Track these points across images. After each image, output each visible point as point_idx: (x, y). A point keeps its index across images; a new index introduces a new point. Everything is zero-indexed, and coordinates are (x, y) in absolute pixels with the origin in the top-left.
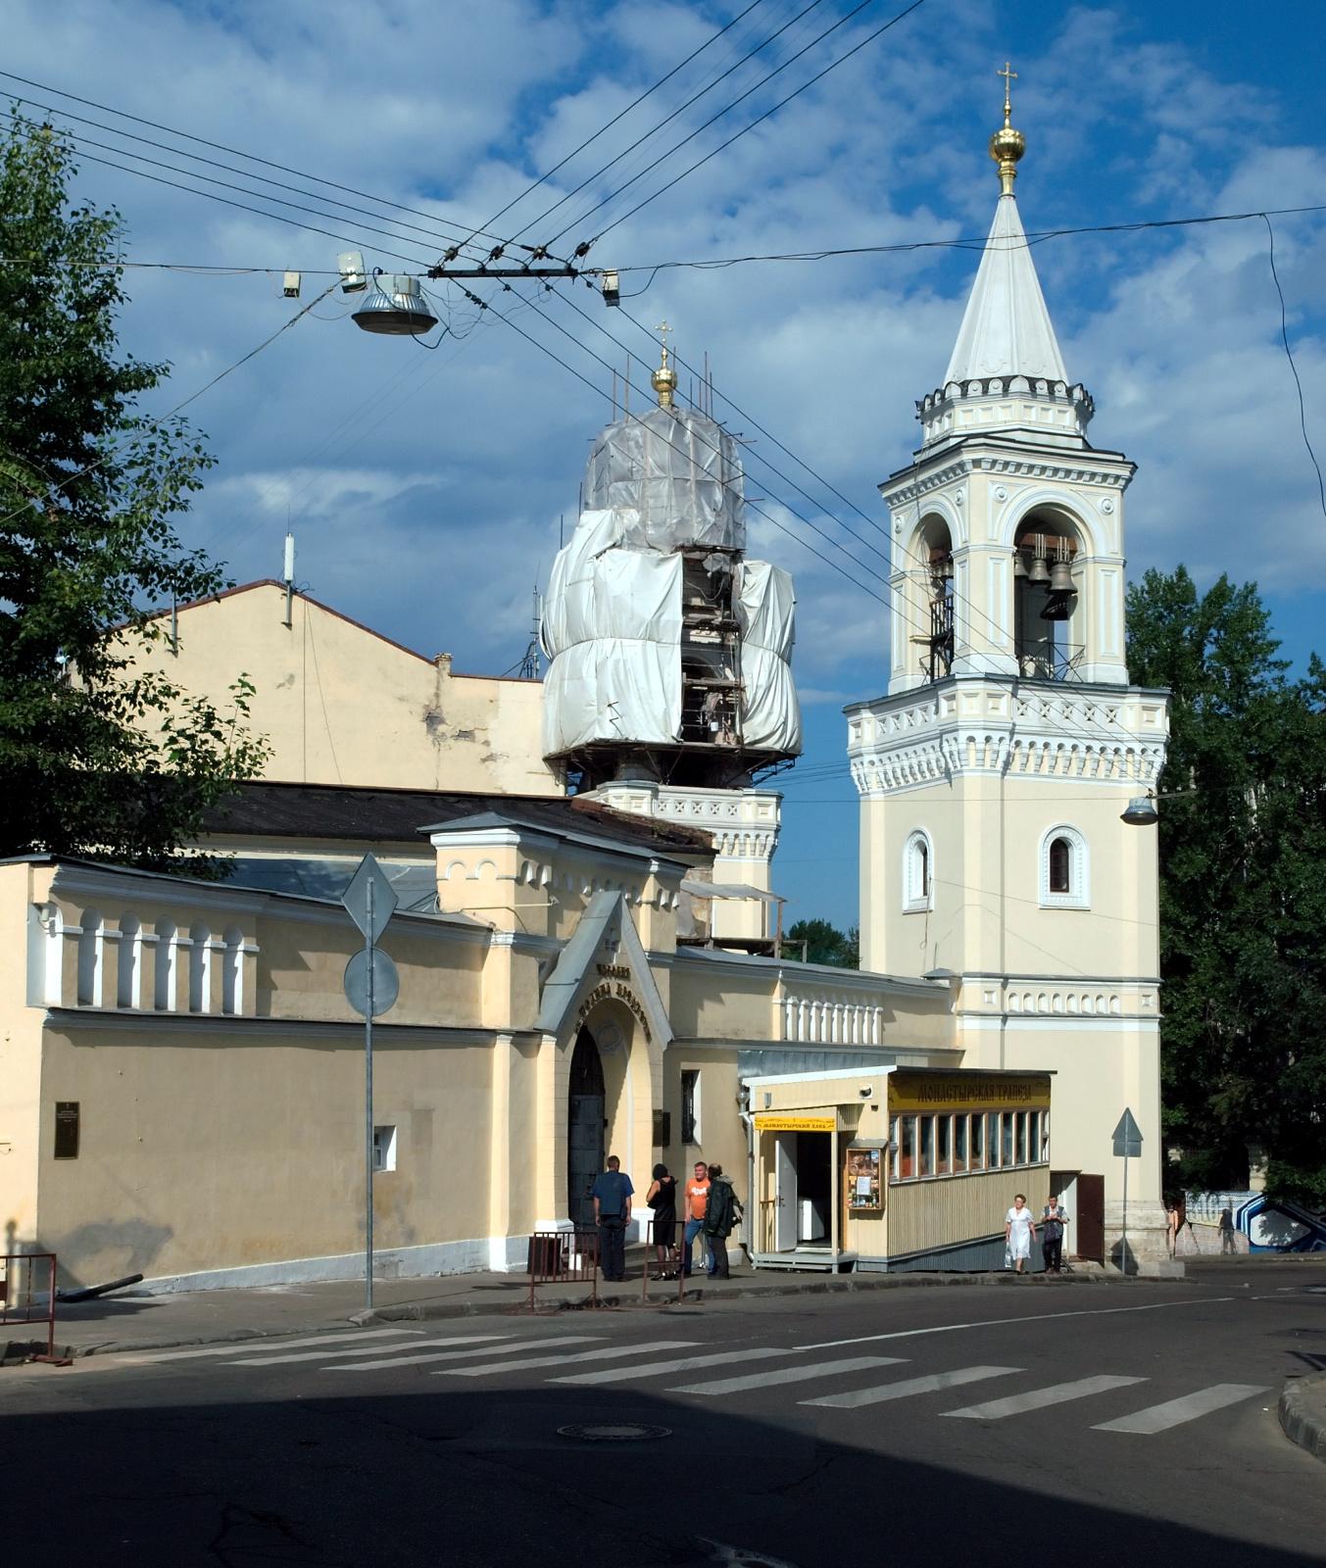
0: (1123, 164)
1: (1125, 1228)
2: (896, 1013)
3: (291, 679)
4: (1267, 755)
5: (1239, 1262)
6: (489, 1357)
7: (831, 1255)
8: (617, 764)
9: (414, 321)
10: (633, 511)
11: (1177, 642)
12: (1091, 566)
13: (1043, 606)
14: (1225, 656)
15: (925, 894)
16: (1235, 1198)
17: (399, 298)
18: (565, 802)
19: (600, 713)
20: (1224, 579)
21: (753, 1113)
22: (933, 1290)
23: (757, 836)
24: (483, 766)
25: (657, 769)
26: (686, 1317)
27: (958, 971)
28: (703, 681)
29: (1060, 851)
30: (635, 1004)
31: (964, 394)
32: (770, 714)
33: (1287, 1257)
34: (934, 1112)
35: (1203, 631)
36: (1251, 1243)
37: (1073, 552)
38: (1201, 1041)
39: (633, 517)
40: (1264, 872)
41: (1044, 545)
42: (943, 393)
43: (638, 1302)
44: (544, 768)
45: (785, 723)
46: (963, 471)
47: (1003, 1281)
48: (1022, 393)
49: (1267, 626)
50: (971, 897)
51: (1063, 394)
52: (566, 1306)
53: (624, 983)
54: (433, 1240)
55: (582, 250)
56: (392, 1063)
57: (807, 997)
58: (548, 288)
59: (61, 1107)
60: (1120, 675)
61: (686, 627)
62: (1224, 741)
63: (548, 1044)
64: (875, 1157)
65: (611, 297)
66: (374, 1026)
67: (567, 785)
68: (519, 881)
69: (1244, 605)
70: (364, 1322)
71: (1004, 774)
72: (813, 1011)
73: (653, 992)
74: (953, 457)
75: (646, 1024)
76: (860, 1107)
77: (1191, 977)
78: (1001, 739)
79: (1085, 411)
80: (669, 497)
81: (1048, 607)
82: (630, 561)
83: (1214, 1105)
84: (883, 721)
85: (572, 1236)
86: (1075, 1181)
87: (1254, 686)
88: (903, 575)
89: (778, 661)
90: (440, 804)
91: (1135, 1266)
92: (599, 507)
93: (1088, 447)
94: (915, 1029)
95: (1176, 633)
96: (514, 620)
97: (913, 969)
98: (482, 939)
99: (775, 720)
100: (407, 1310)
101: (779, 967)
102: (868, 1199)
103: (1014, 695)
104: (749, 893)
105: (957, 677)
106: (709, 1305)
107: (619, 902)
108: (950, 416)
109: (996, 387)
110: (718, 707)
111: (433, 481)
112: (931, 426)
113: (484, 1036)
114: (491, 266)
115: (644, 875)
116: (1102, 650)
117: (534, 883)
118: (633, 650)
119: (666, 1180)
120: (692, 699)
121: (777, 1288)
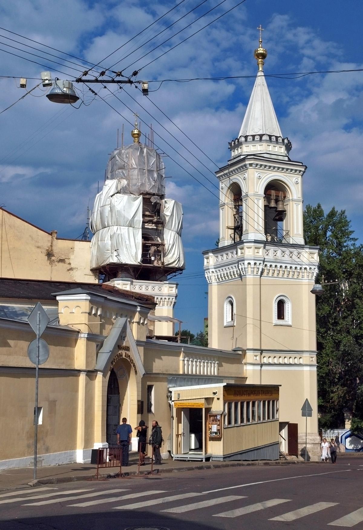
0: (291, 67)
1: (306, 444)
2: (223, 363)
4: (350, 271)
5: (342, 455)
6: (87, 499)
7: (202, 455)
8: (118, 272)
9: (70, 98)
10: (124, 180)
11: (318, 231)
12: (291, 202)
13: (274, 216)
15: (232, 320)
16: (340, 432)
17: (65, 89)
18: (100, 285)
19: (112, 253)
20: (334, 209)
21: (173, 401)
22: (241, 468)
23: (169, 299)
24: (68, 272)
25: (132, 274)
26: (156, 480)
27: (245, 348)
28: (150, 242)
29: (281, 304)
30: (132, 360)
31: (246, 140)
32: (174, 254)
33: (359, 453)
34: (239, 401)
36: (346, 449)
37: (285, 197)
38: (327, 374)
39: (124, 182)
40: (349, 313)
41: (275, 195)
42: (238, 140)
43: (136, 474)
44: (91, 273)
45: (179, 257)
46: (246, 167)
47: (266, 464)
48: (266, 140)
49: (350, 226)
50: (249, 321)
51: (281, 141)
52: (110, 477)
53: (127, 352)
54: (55, 451)
55: (135, 73)
56: (45, 382)
57: (196, 358)
58: (121, 88)
60: (301, 241)
61: (144, 222)
62: (335, 267)
63: (100, 375)
64: (219, 417)
65: (145, 91)
66: (39, 369)
67: (99, 279)
68: (90, 314)
70: (34, 485)
71: (261, 276)
72: (194, 363)
73: (137, 356)
74: (243, 162)
75: (135, 367)
76: (213, 398)
77: (324, 351)
78: (260, 264)
79: (288, 147)
80: (138, 176)
81: (276, 216)
82: (124, 198)
83: (332, 397)
84: (217, 257)
85: (108, 449)
86: (287, 426)
87: (345, 247)
88: (224, 204)
89: (177, 235)
90: (53, 285)
91: (309, 458)
92: (112, 178)
93: (289, 160)
94: (229, 369)
95: (317, 228)
96: (78, 221)
97: (228, 347)
98: (75, 336)
99: (176, 256)
100: (50, 480)
101: (182, 346)
102: (216, 433)
103: (264, 248)
104: (167, 319)
105: (244, 241)
106: (163, 475)
107: (126, 322)
108: (241, 148)
109: (257, 138)
110: (155, 251)
111: (48, 171)
112: (234, 151)
113: (76, 372)
115: (134, 313)
116: (295, 232)
117: (95, 315)
118: (124, 230)
119: (144, 427)
120: (145, 248)
121: (186, 468)
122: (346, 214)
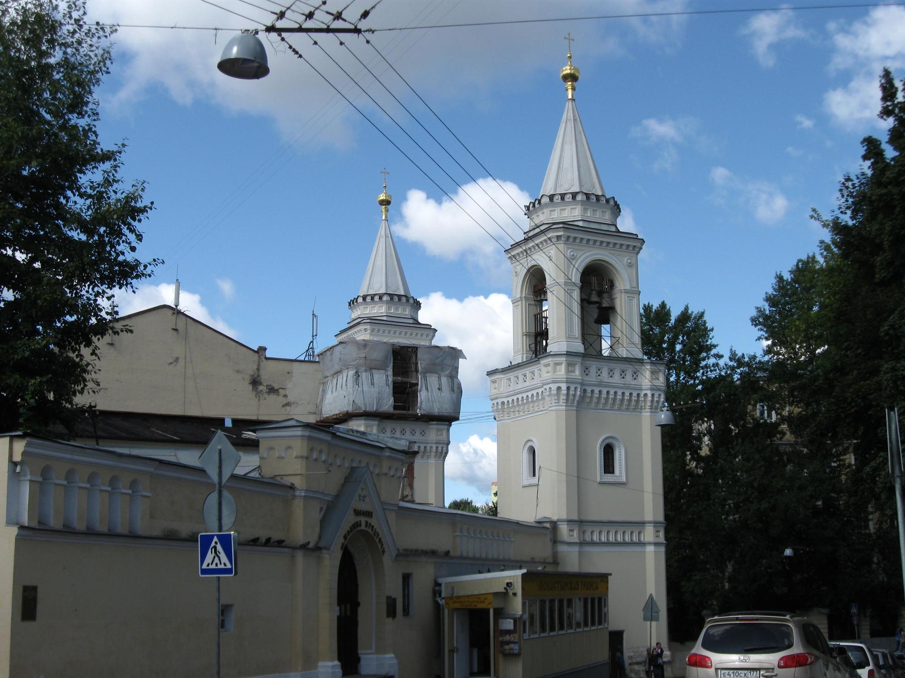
3: (177, 360)
14: (687, 349)
20: (687, 308)
29: (609, 451)
35: (676, 338)
55: (365, 15)
59: (26, 589)
69: (696, 323)
114: (306, 25)
122: (706, 318)
